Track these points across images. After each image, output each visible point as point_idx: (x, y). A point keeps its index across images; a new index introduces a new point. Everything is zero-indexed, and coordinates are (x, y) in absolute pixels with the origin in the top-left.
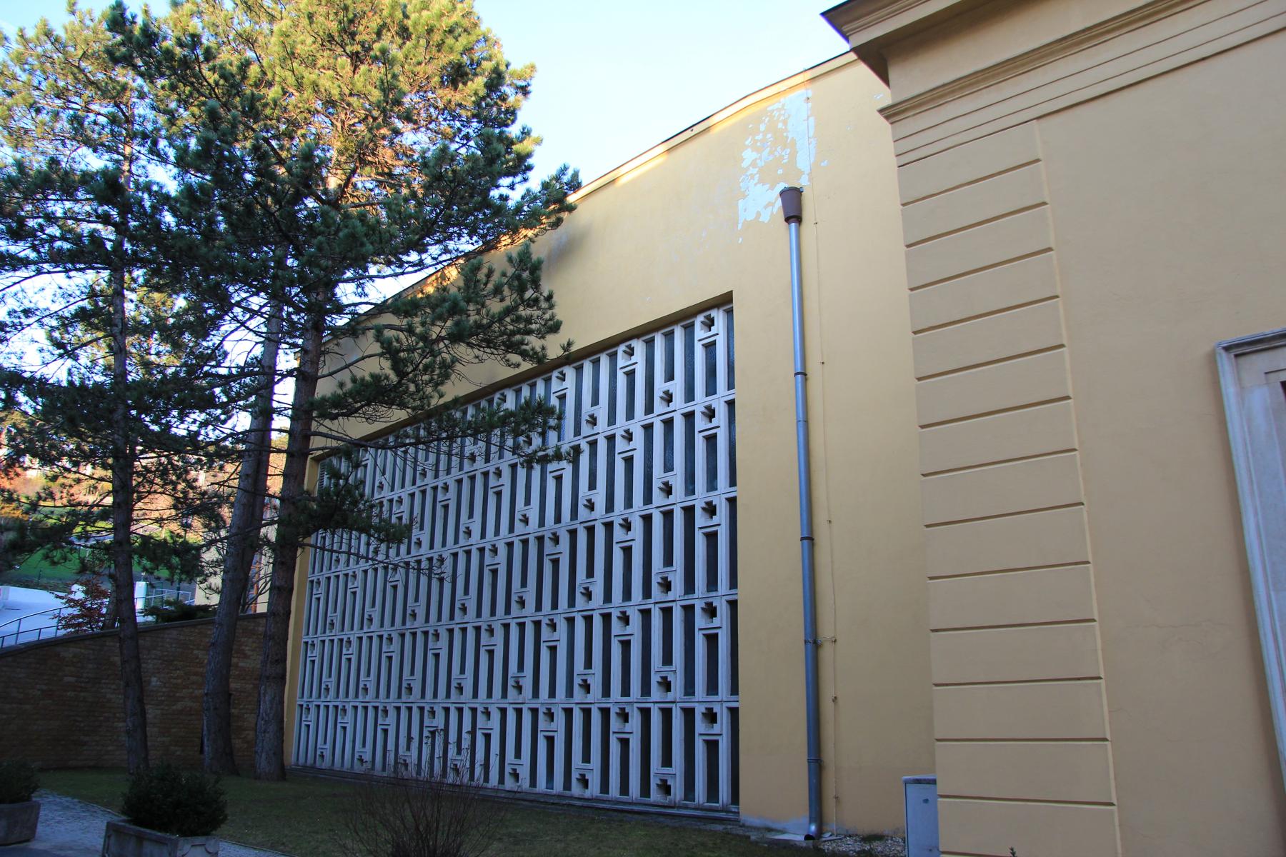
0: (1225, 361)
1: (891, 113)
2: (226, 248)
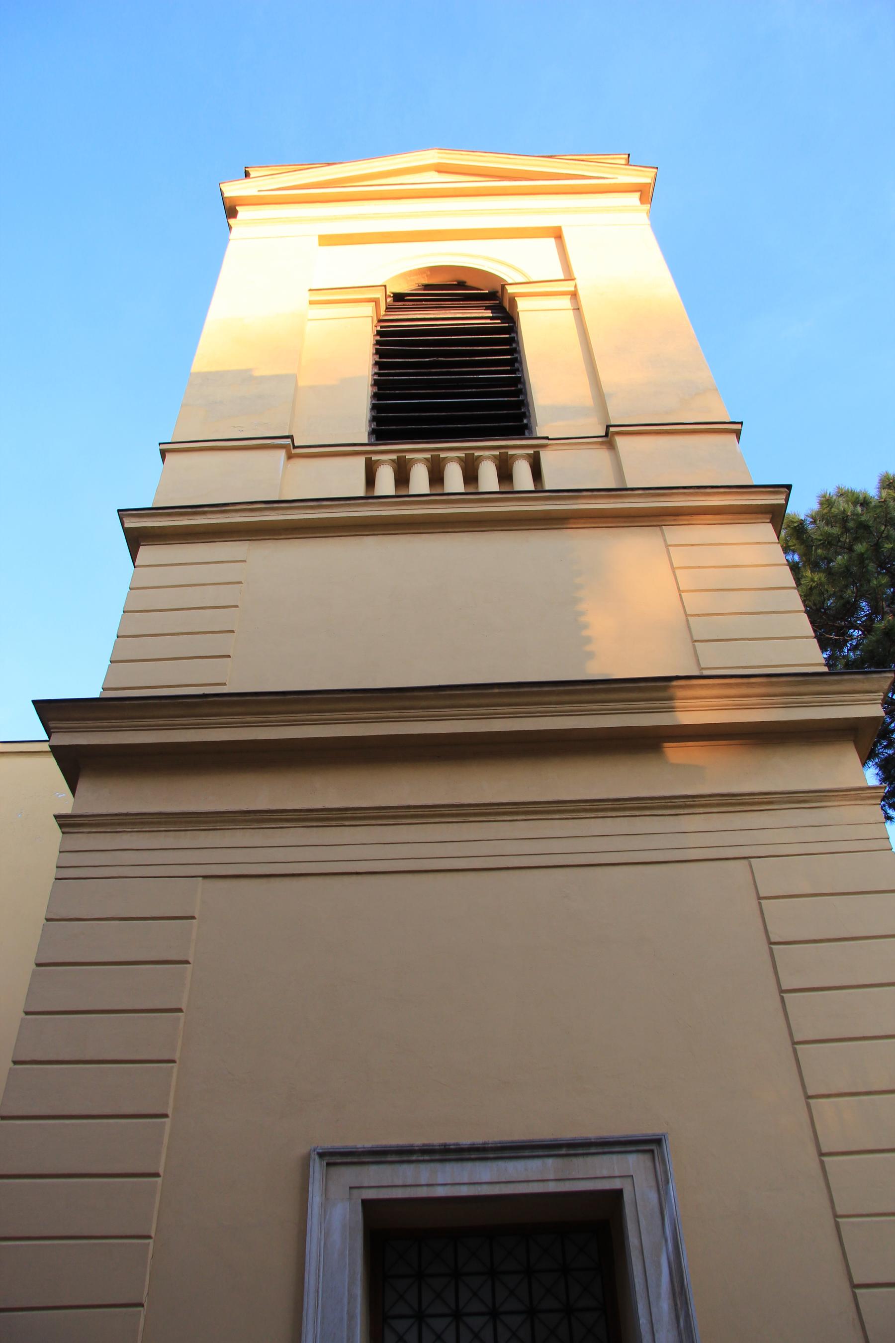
0: (317, 1168)
1: (66, 822)
2: (811, 581)
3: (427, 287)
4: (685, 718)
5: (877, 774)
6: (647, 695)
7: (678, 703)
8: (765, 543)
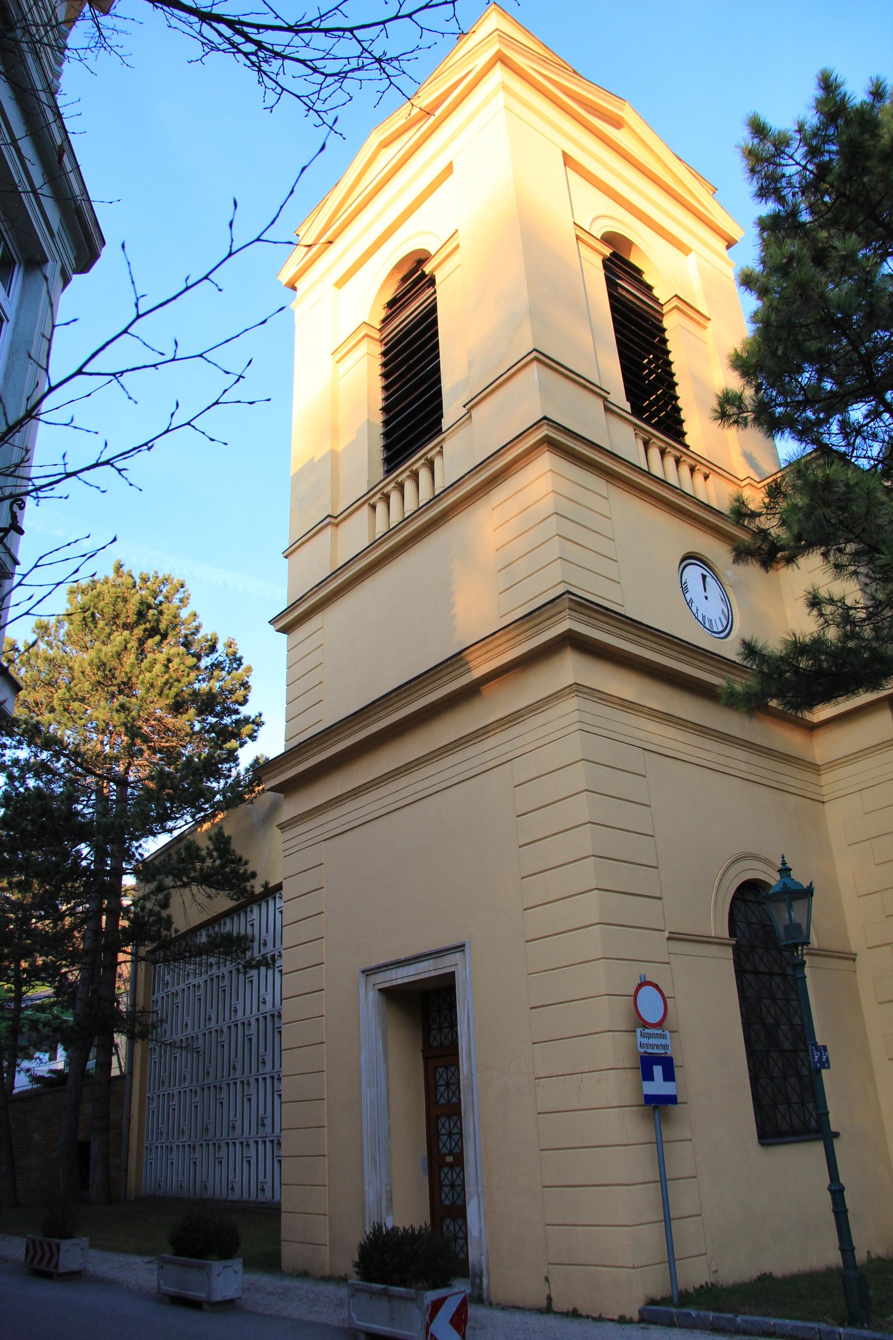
3: (404, 280)
4: (477, 673)
5: (246, 863)
6: (456, 666)
7: (471, 665)
8: (543, 475)
